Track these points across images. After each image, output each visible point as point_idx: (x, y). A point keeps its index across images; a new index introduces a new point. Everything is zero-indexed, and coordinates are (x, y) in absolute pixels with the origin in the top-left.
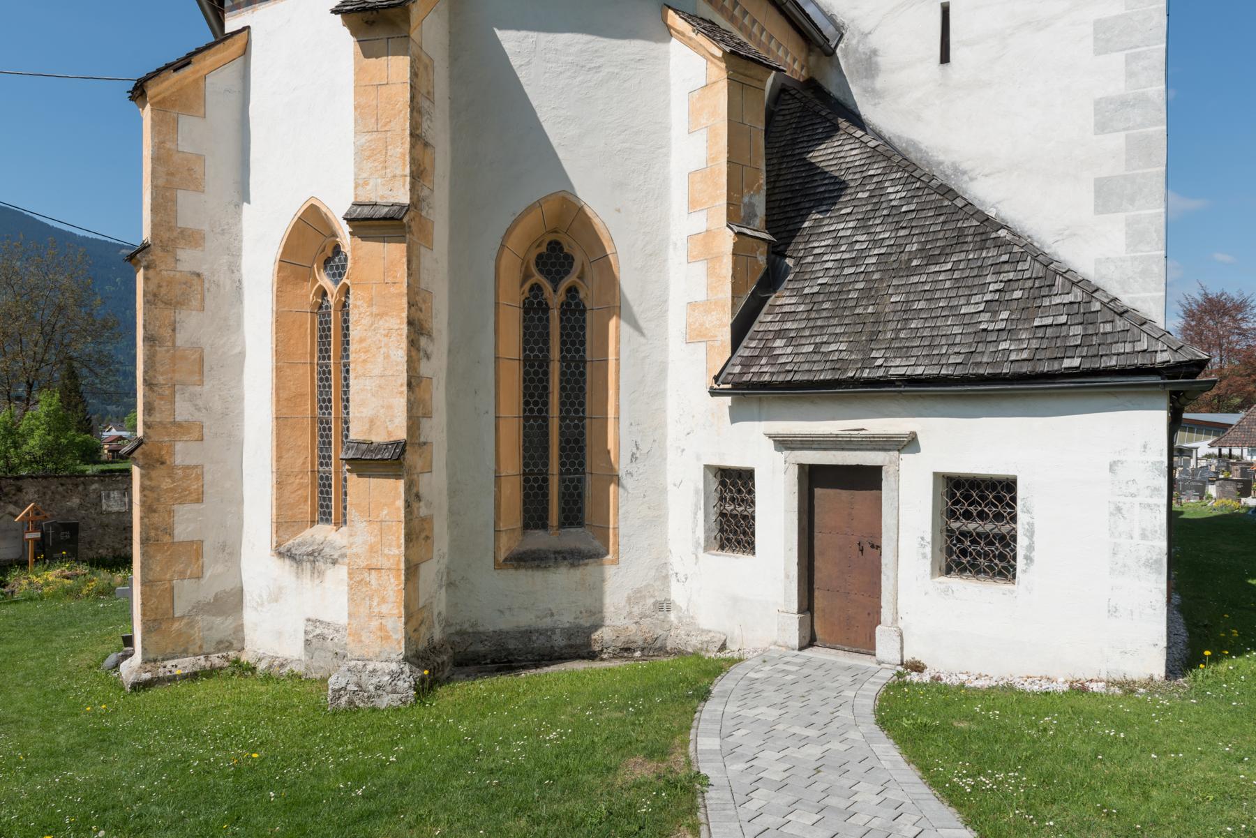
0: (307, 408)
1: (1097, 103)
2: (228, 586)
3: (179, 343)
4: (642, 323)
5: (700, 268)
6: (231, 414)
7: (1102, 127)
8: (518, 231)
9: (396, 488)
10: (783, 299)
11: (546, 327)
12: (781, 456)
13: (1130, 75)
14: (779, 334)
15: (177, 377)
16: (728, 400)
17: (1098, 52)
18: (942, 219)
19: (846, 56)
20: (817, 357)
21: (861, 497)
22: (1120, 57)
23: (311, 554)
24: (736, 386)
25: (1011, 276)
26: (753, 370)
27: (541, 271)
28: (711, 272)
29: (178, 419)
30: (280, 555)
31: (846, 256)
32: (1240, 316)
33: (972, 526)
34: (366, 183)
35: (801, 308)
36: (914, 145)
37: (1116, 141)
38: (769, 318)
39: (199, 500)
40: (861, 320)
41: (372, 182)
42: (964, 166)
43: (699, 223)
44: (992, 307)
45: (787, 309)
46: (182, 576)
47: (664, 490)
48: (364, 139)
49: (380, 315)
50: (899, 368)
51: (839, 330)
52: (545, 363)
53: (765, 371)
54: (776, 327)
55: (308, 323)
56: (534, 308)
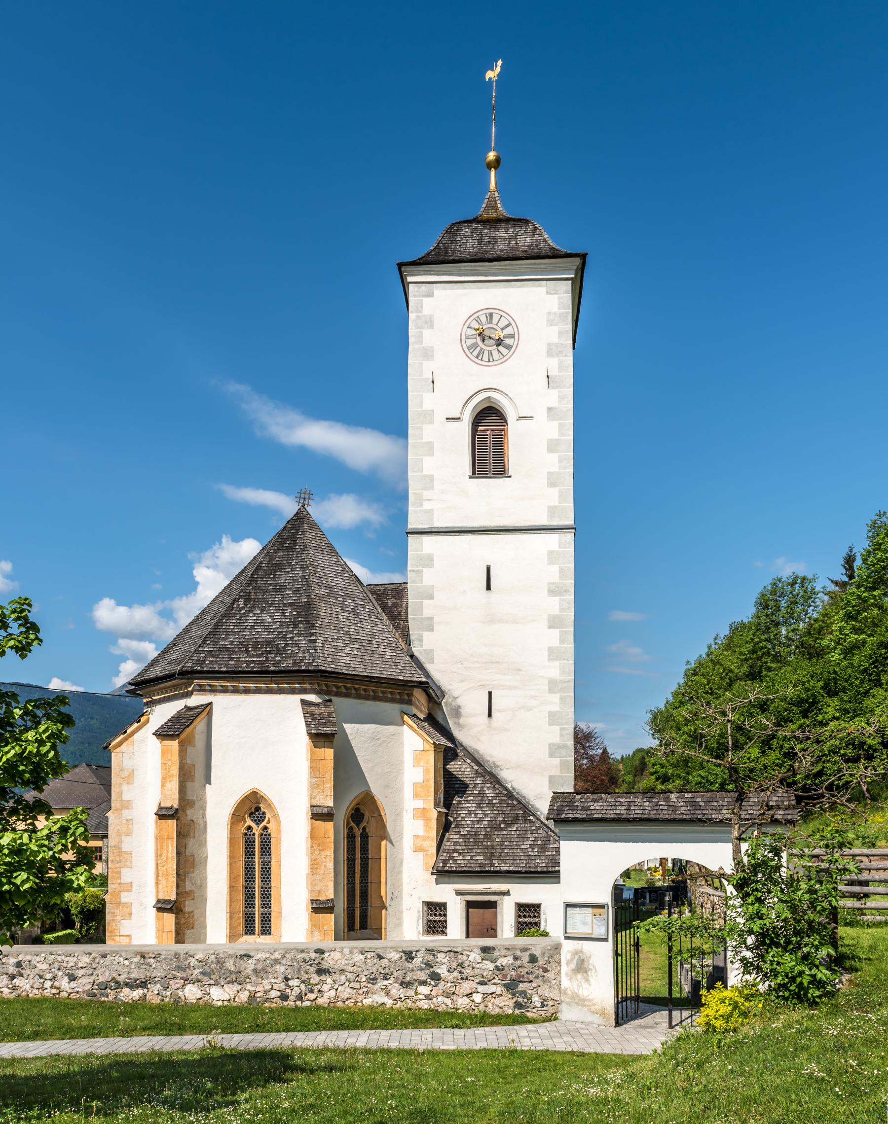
0: (241, 882)
1: (550, 745)
4: (394, 843)
5: (420, 823)
7: (551, 755)
9: (331, 918)
10: (452, 836)
11: (354, 845)
12: (458, 898)
13: (561, 735)
14: (455, 851)
15: (186, 870)
16: (435, 876)
17: (550, 724)
18: (509, 808)
19: (446, 706)
20: (472, 862)
21: (490, 911)
22: (558, 728)
24: (438, 871)
25: (536, 835)
26: (448, 865)
29: (187, 890)
31: (475, 819)
32: (588, 745)
34: (315, 797)
35: (461, 840)
36: (477, 751)
37: (556, 761)
38: (449, 844)
39: (193, 928)
40: (486, 847)
41: (318, 797)
42: (498, 763)
43: (420, 804)
44: (532, 847)
45: (455, 840)
47: (402, 912)
48: (314, 780)
49: (323, 850)
50: (504, 867)
52: (354, 859)
53: (451, 865)
54: (452, 848)
55: (241, 842)
56: (351, 837)
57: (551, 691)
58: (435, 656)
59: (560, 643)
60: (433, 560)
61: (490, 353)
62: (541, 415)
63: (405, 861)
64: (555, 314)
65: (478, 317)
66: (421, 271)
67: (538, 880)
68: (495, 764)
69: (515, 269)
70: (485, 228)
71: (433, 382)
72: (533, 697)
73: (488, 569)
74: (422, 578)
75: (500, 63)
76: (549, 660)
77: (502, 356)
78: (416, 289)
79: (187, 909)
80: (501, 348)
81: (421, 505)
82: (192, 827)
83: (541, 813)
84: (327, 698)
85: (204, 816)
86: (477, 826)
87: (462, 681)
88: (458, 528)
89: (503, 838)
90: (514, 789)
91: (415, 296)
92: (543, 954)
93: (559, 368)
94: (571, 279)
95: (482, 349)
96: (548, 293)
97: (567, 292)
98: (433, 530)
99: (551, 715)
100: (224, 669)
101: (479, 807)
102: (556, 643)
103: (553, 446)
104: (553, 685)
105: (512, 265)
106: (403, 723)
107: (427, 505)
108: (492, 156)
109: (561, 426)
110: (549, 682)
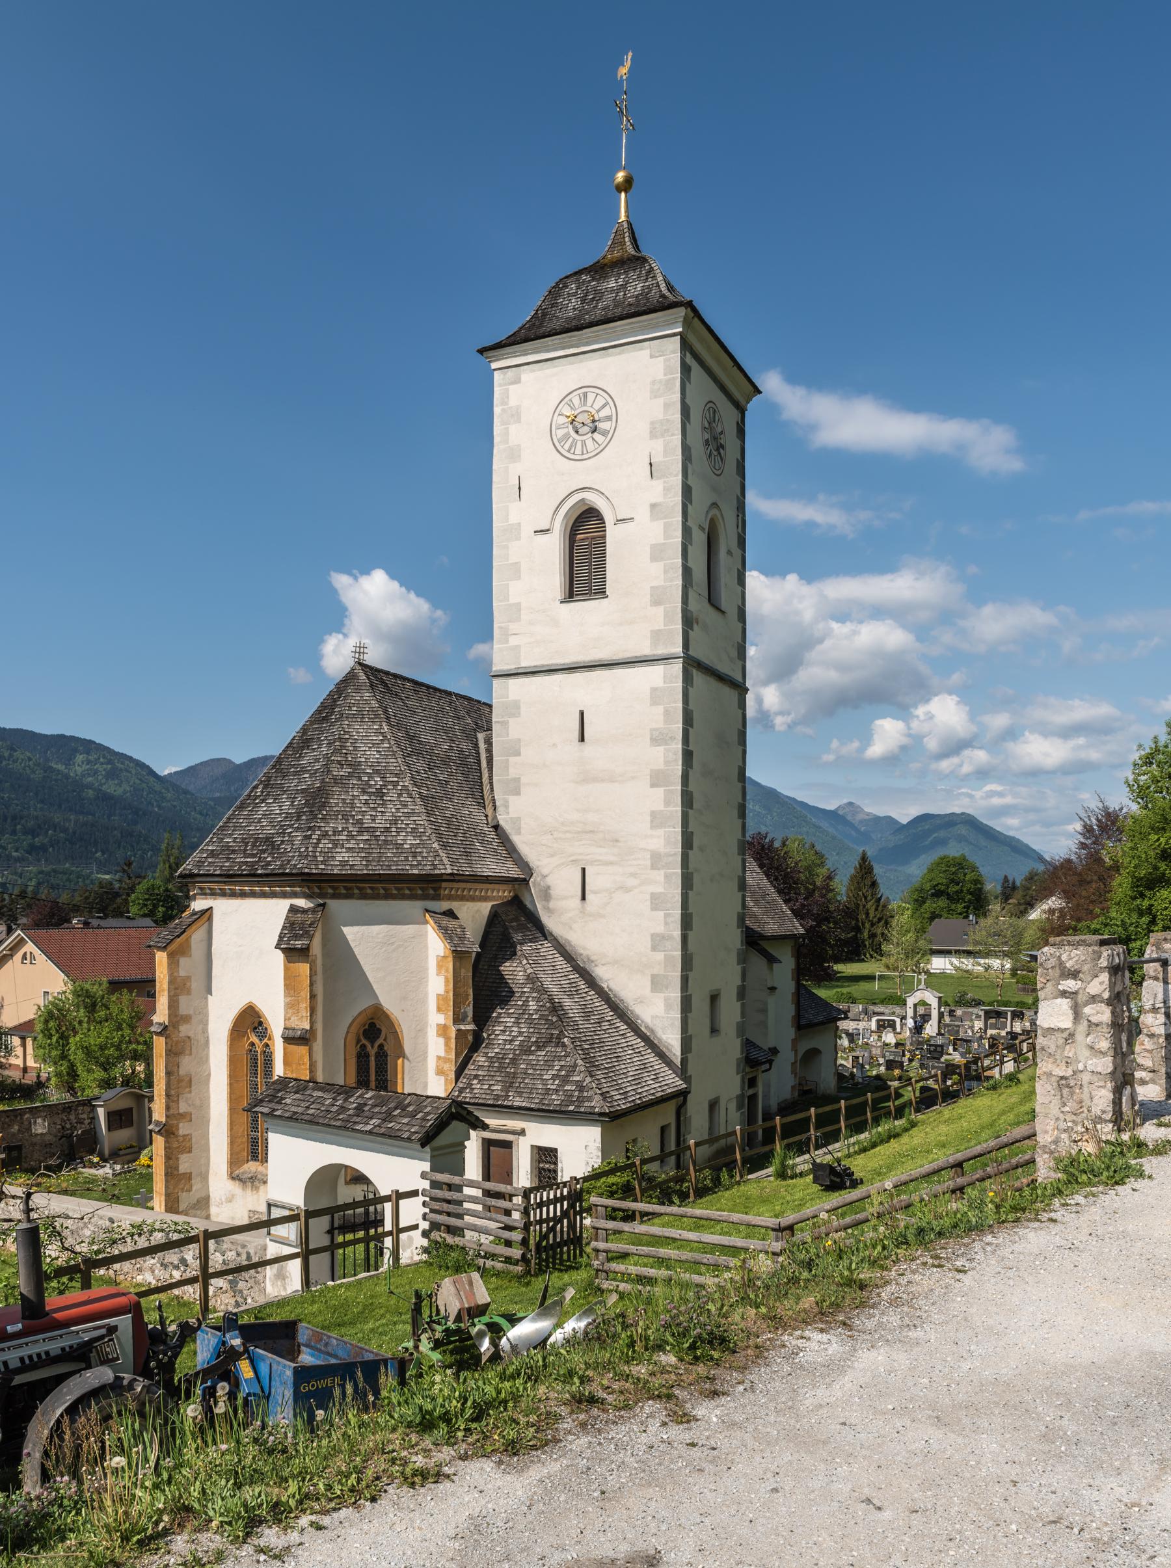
1: (652, 935)
2: (203, 1195)
3: (180, 1073)
5: (441, 1041)
6: (204, 1105)
8: (355, 1024)
10: (480, 1058)
11: (368, 1065)
13: (666, 924)
17: (652, 909)
19: (534, 886)
20: (488, 1092)
22: (662, 913)
23: (251, 1178)
27: (365, 1038)
28: (447, 1044)
29: (181, 1111)
30: (233, 1178)
31: (508, 1038)
33: (547, 1166)
36: (569, 942)
37: (660, 956)
39: (190, 1152)
42: (593, 958)
44: (554, 1077)
45: (480, 1064)
46: (182, 1190)
48: (289, 999)
51: (499, 1079)
54: (474, 1073)
55: (245, 1061)
56: (362, 1057)
57: (654, 867)
58: (523, 826)
59: (665, 806)
60: (519, 708)
61: (584, 444)
62: (642, 514)
63: (429, 1084)
64: (660, 381)
65: (571, 400)
66: (515, 353)
67: (554, 1120)
68: (589, 959)
69: (610, 333)
70: (593, 280)
71: (520, 488)
72: (634, 875)
73: (582, 714)
74: (508, 730)
75: (630, 55)
76: (652, 827)
77: (597, 446)
78: (502, 376)
79: (181, 1132)
80: (596, 435)
81: (507, 642)
82: (188, 1044)
83: (642, 1022)
84: (321, 901)
85: (205, 1030)
86: (508, 1047)
87: (552, 856)
88: (548, 665)
89: (529, 1064)
90: (610, 990)
91: (500, 385)
92: (256, 1253)
93: (665, 451)
94: (680, 334)
95: (574, 439)
96: (652, 356)
97: (674, 352)
98: (520, 671)
99: (654, 897)
100: (218, 872)
101: (517, 1023)
102: (659, 806)
103: (657, 553)
104: (656, 860)
105: (605, 329)
106: (427, 922)
107: (513, 641)
108: (620, 176)
109: (667, 527)
110: (652, 857)
